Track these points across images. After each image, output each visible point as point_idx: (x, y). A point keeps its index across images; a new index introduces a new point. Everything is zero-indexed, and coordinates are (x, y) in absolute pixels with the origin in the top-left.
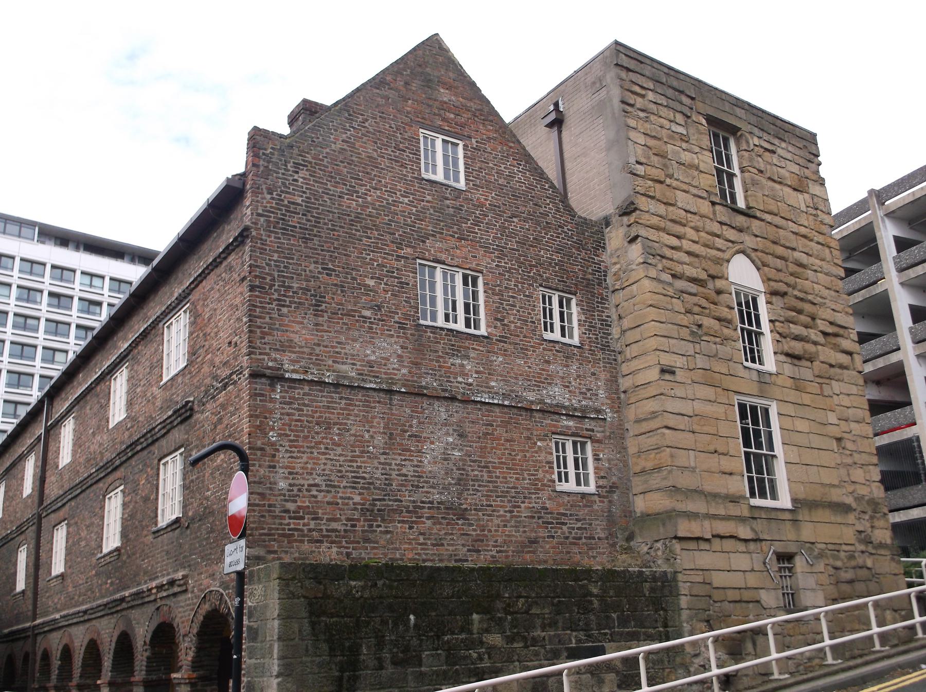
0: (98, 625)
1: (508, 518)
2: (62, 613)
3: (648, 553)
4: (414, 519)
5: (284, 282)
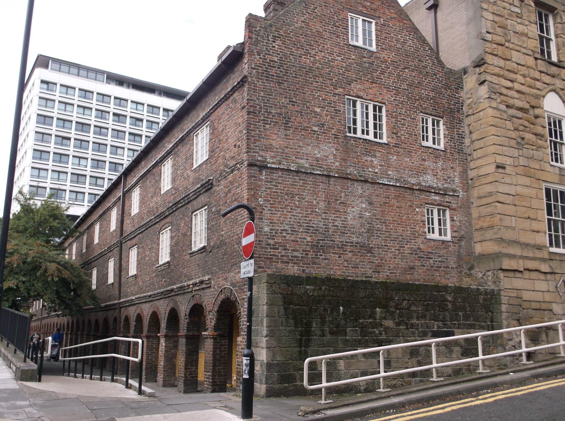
0: (157, 304)
1: (397, 254)
2: (136, 296)
3: (482, 278)
4: (342, 252)
5: (267, 109)
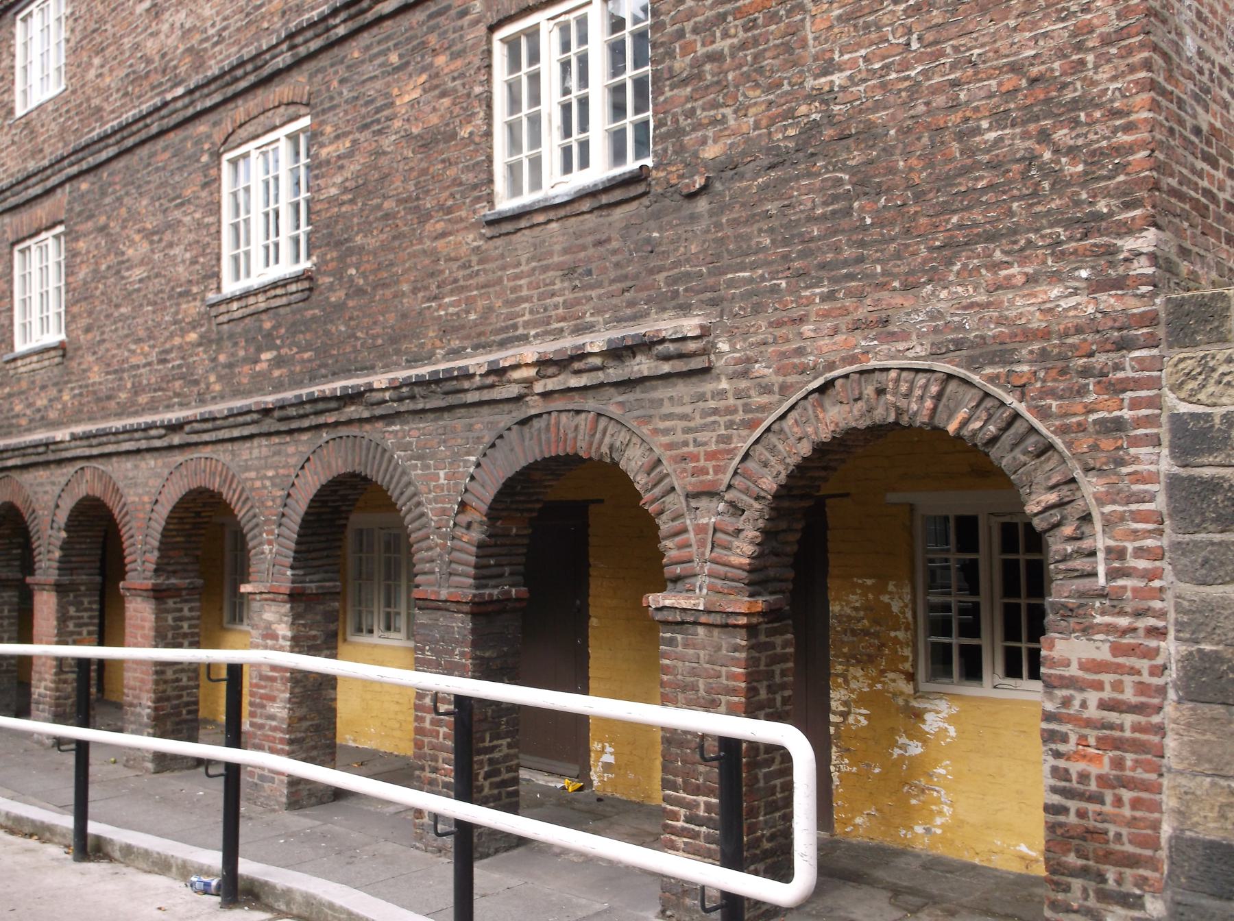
2: (79, 429)
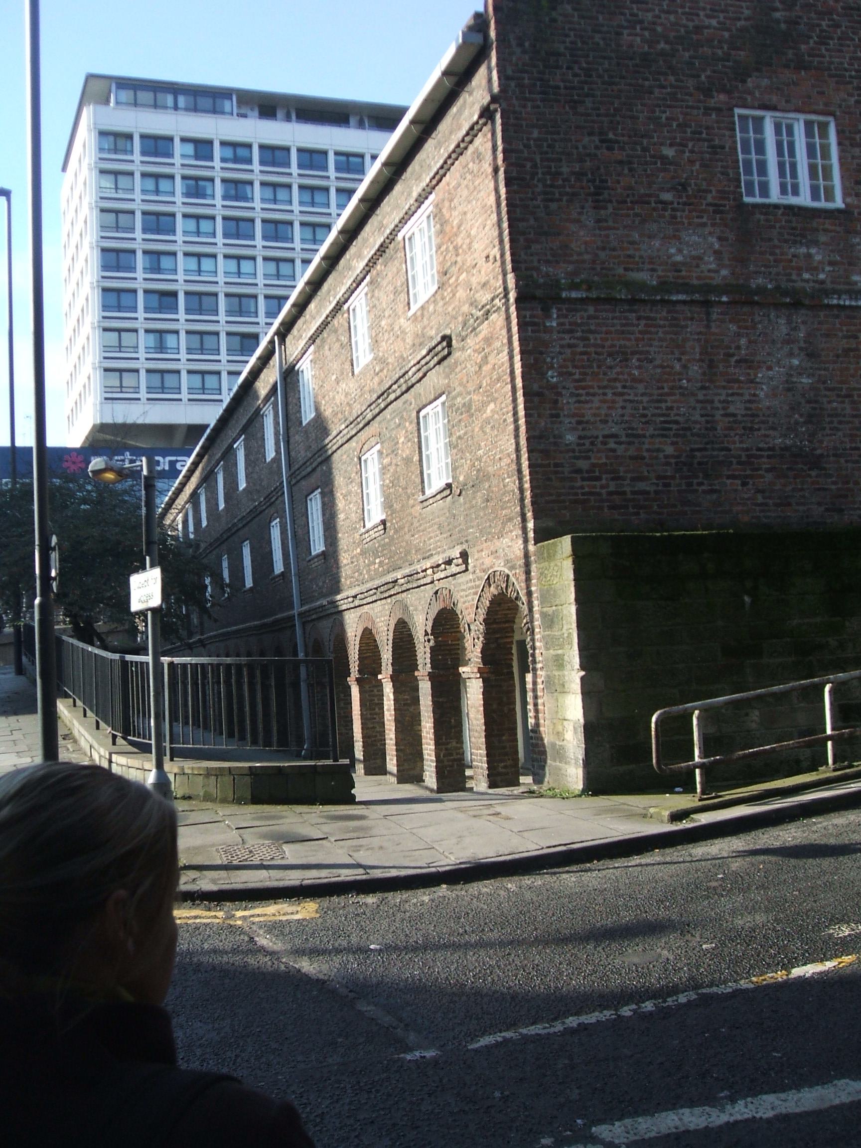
4: (748, 472)
